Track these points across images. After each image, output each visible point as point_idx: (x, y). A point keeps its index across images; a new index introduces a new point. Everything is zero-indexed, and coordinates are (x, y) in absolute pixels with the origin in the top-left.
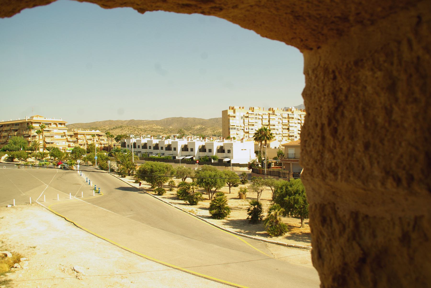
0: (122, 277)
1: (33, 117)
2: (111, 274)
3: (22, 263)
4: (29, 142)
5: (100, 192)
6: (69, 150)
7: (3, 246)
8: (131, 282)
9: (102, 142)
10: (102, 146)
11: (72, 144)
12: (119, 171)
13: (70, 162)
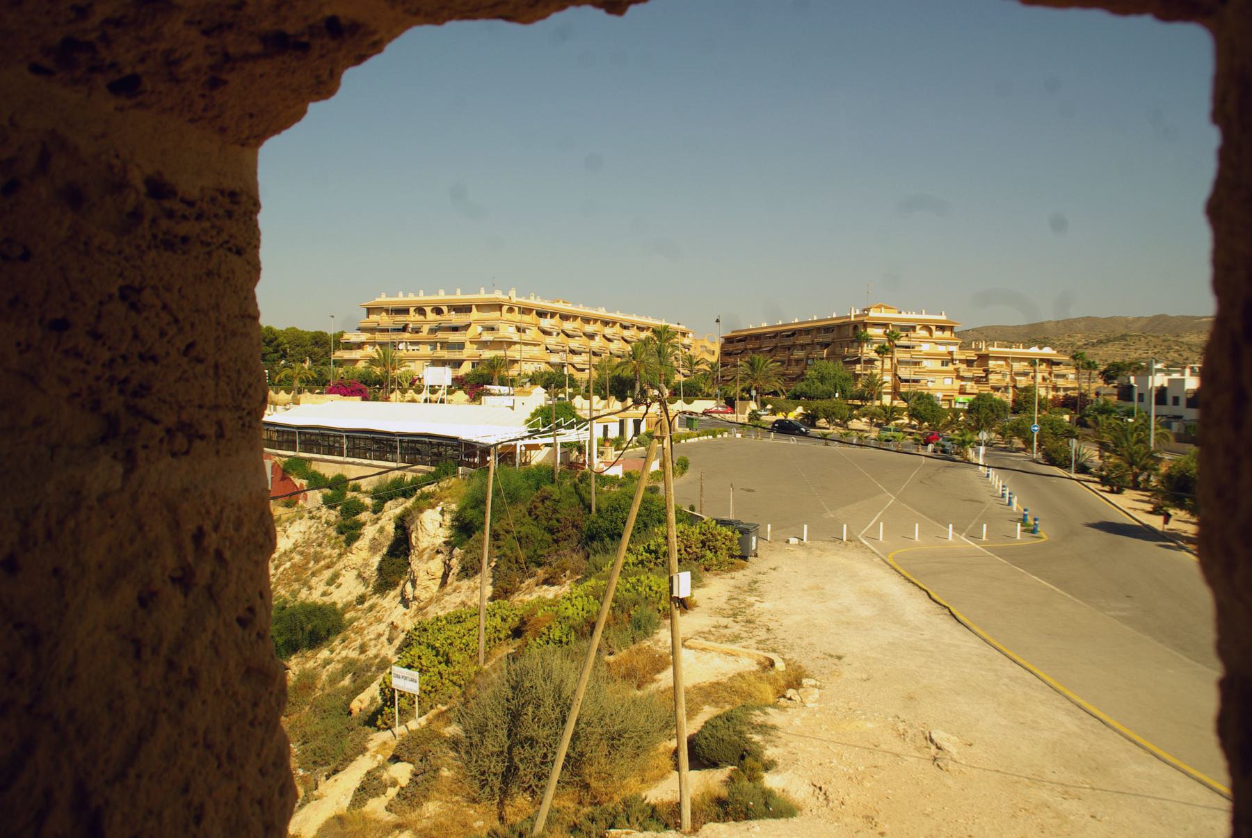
0: (1066, 792)
1: (868, 310)
2: (1033, 775)
3: (806, 691)
4: (857, 376)
5: (1039, 529)
6: (962, 402)
7: (768, 639)
8: (1092, 817)
9: (1061, 382)
10: (1059, 393)
11: (970, 387)
12: (1104, 473)
13: (961, 436)
